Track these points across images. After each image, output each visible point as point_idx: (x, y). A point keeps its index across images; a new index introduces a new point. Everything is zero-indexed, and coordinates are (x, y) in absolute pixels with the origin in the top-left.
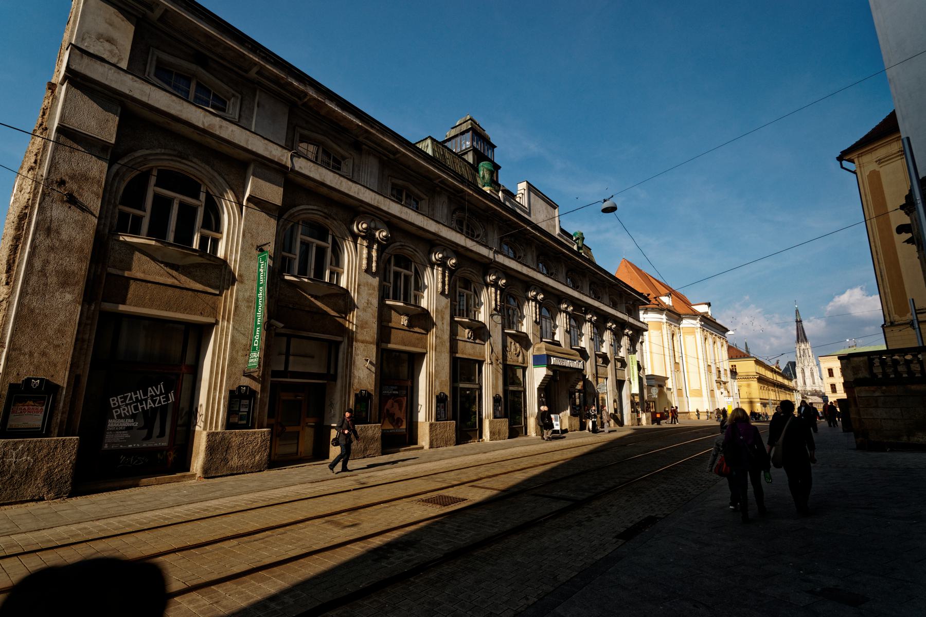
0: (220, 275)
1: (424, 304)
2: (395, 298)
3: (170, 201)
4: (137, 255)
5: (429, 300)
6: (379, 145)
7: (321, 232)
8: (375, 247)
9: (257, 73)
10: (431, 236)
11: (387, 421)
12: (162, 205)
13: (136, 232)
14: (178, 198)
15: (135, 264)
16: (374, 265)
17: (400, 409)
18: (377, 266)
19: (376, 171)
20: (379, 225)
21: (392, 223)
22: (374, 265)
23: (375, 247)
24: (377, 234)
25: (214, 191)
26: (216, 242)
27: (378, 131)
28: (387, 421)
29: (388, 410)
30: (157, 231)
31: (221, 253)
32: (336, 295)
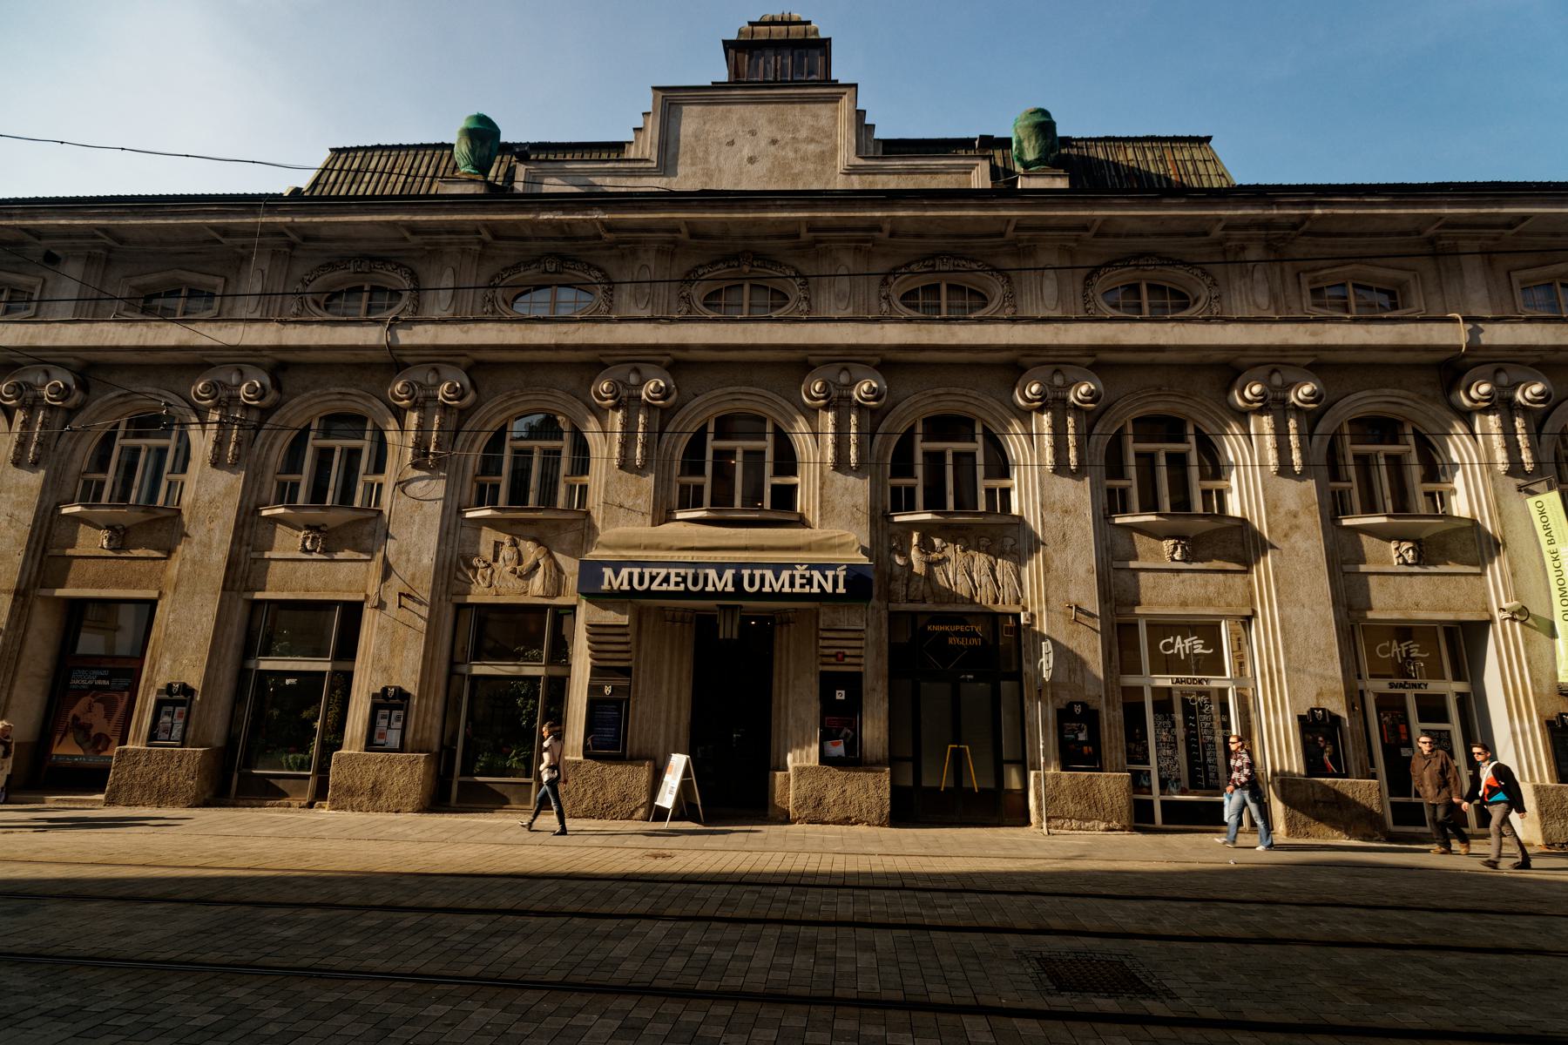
0: (1240, 545)
1: (1460, 506)
2: (1370, 508)
3: (941, 455)
4: (1364, 538)
5: (1241, 497)
6: (69, 236)
7: (1172, 428)
8: (1292, 423)
9: (809, 230)
10: (1005, 355)
11: (70, 737)
12: (1147, 462)
13: (911, 507)
14: (1163, 449)
15: (80, 540)
16: (1072, 454)
17: (108, 715)
18: (1535, 456)
19: (1483, 292)
20: (1290, 376)
21: (1320, 362)
22: (1072, 454)
23: (1292, 423)
24: (1519, 396)
25: (1209, 428)
26: (1221, 495)
27: (22, 216)
28: (70, 737)
29: (75, 718)
30: (934, 501)
31: (1015, 510)
32: (1231, 529)
